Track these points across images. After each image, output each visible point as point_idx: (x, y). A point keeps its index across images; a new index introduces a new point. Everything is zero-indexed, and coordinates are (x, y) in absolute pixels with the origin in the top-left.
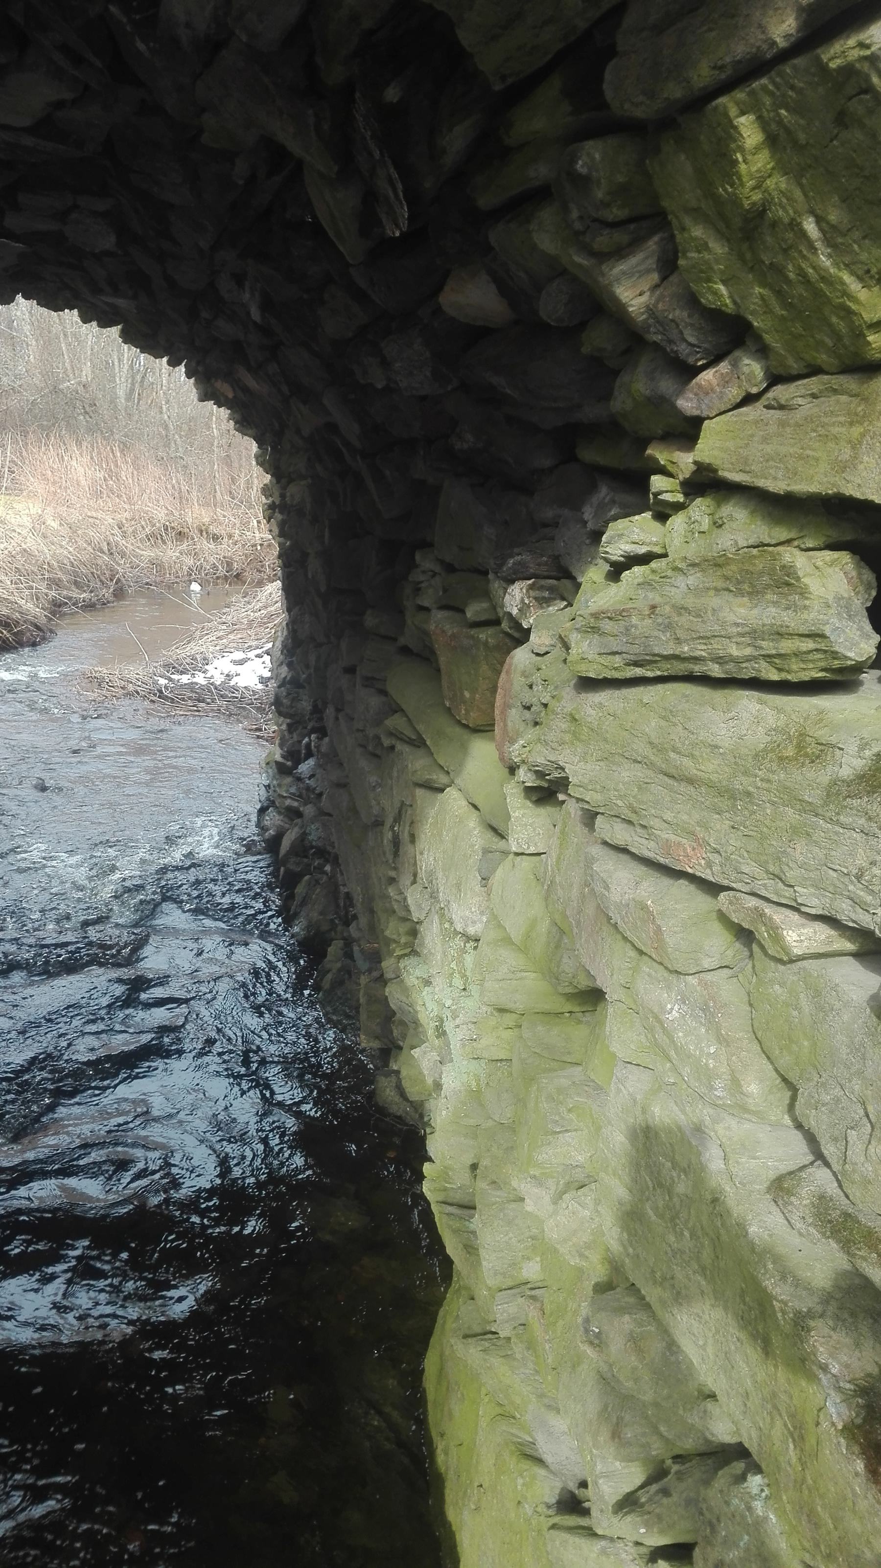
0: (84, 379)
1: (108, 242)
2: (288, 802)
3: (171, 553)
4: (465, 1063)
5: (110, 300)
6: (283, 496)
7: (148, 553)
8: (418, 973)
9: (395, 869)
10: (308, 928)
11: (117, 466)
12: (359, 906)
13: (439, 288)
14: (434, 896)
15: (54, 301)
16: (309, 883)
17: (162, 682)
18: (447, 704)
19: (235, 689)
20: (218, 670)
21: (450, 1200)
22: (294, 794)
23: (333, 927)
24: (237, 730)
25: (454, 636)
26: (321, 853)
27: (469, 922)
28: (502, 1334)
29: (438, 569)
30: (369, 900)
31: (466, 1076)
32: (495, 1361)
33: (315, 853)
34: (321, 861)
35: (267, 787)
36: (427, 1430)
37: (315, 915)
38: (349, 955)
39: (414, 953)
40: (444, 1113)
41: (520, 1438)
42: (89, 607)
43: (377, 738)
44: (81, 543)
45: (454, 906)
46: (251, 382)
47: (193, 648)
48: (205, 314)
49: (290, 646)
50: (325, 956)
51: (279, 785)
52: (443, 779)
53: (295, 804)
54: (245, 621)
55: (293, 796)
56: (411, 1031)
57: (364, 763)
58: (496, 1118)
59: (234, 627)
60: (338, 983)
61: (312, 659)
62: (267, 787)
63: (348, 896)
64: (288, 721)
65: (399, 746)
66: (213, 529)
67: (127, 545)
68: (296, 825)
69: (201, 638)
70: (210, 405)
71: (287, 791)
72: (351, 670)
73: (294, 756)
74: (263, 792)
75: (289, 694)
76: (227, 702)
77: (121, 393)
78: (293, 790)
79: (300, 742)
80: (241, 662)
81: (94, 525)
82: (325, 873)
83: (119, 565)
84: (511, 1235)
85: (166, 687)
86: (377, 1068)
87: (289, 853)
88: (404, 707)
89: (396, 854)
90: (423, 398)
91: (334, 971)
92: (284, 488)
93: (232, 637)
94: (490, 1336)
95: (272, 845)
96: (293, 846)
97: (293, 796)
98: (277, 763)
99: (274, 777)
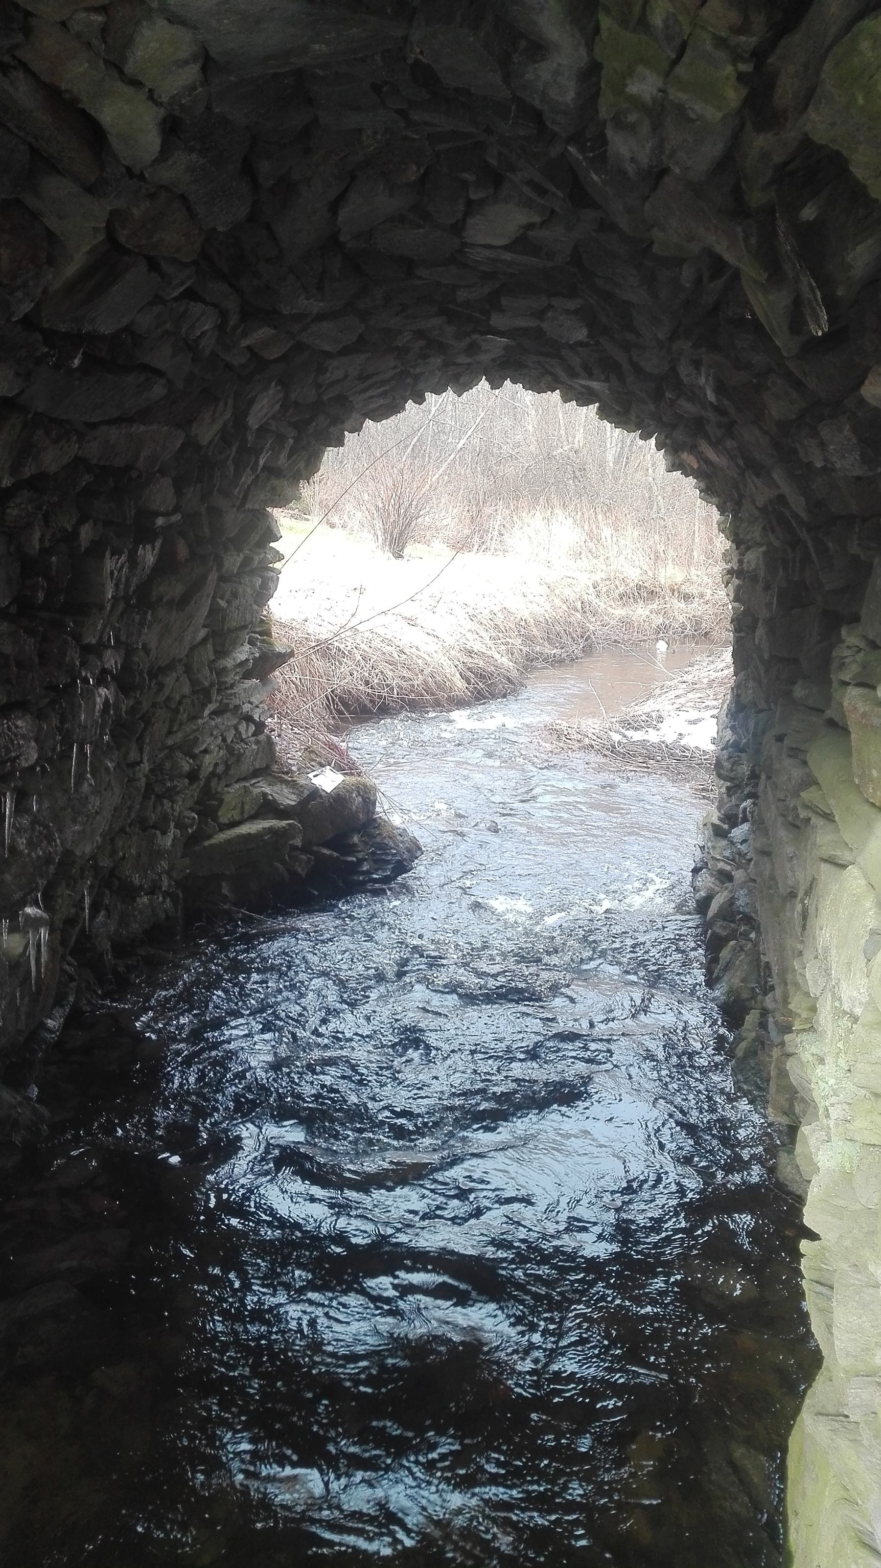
0: (576, 446)
1: (581, 334)
2: (721, 865)
3: (641, 612)
4: (841, 1143)
5: (583, 382)
6: (740, 562)
7: (619, 612)
8: (814, 1050)
9: (802, 942)
10: (729, 993)
11: (598, 527)
12: (775, 976)
13: (862, 383)
14: (827, 972)
15: (537, 385)
16: (734, 949)
17: (616, 737)
18: (857, 781)
19: (685, 748)
20: (667, 733)
21: (823, 1280)
22: (728, 858)
23: (753, 997)
24: (686, 791)
25: (864, 715)
26: (748, 919)
27: (857, 1003)
28: (852, 1418)
29: (862, 645)
30: (784, 971)
31: (840, 1156)
32: (842, 1443)
33: (741, 919)
34: (747, 928)
35: (702, 848)
36: (785, 1507)
37: (736, 982)
38: (763, 1025)
39: (812, 1029)
40: (816, 1190)
41: (860, 1525)
42: (558, 662)
43: (795, 808)
44: (557, 601)
45: (843, 984)
46: (712, 455)
47: (649, 706)
48: (668, 395)
49: (733, 710)
50: (743, 1024)
51: (714, 847)
52: (847, 856)
53: (728, 868)
54: (705, 681)
55: (726, 860)
56: (811, 1109)
57: (782, 833)
58: (863, 1201)
59: (693, 687)
60: (751, 1053)
61: (751, 724)
62: (702, 848)
63: (768, 965)
64: (729, 784)
65: (814, 820)
66: (685, 589)
67: (601, 604)
68: (726, 888)
69: (660, 695)
70: (678, 474)
71: (721, 854)
72: (780, 739)
73: (732, 819)
74: (698, 852)
75: (730, 758)
76: (673, 760)
77: (610, 457)
78: (727, 853)
79: (738, 806)
80: (694, 722)
81: (570, 585)
82: (750, 940)
83: (591, 623)
84: (864, 1319)
85: (619, 742)
86: (783, 1144)
87: (716, 916)
88: (820, 780)
89: (804, 927)
90: (859, 478)
91: (749, 1040)
92: (742, 554)
93: (690, 695)
94: (842, 1418)
95: (703, 906)
96: (721, 909)
97: (726, 860)
98: (713, 825)
99: (709, 839)
